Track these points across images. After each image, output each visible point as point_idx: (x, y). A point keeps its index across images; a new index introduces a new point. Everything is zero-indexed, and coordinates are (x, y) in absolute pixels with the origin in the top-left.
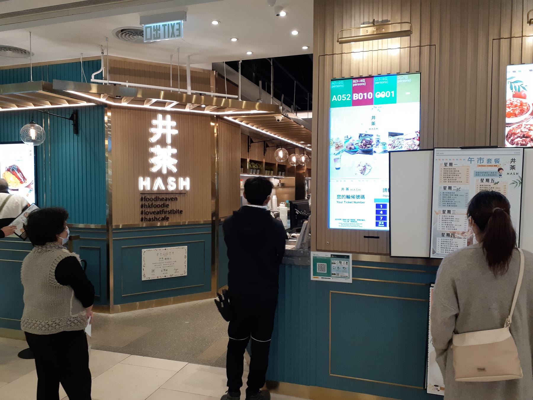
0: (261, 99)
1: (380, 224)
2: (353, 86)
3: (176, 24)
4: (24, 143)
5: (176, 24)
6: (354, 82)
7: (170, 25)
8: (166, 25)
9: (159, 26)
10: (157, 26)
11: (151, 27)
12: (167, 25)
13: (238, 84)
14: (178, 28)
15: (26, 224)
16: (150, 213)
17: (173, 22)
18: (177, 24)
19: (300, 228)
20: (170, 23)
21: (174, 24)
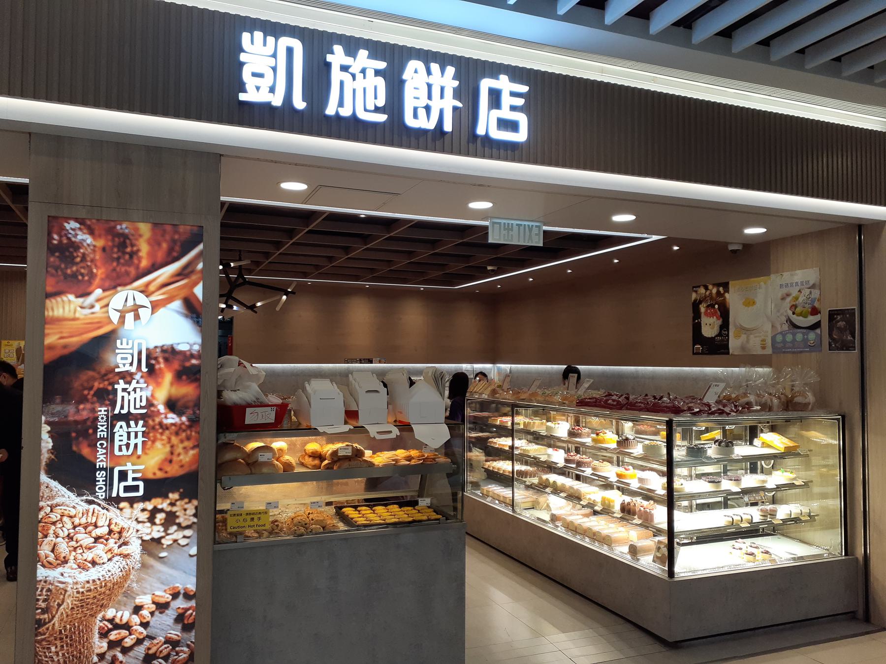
11: (500, 223)
12: (523, 225)
17: (531, 224)
18: (536, 226)
20: (527, 223)
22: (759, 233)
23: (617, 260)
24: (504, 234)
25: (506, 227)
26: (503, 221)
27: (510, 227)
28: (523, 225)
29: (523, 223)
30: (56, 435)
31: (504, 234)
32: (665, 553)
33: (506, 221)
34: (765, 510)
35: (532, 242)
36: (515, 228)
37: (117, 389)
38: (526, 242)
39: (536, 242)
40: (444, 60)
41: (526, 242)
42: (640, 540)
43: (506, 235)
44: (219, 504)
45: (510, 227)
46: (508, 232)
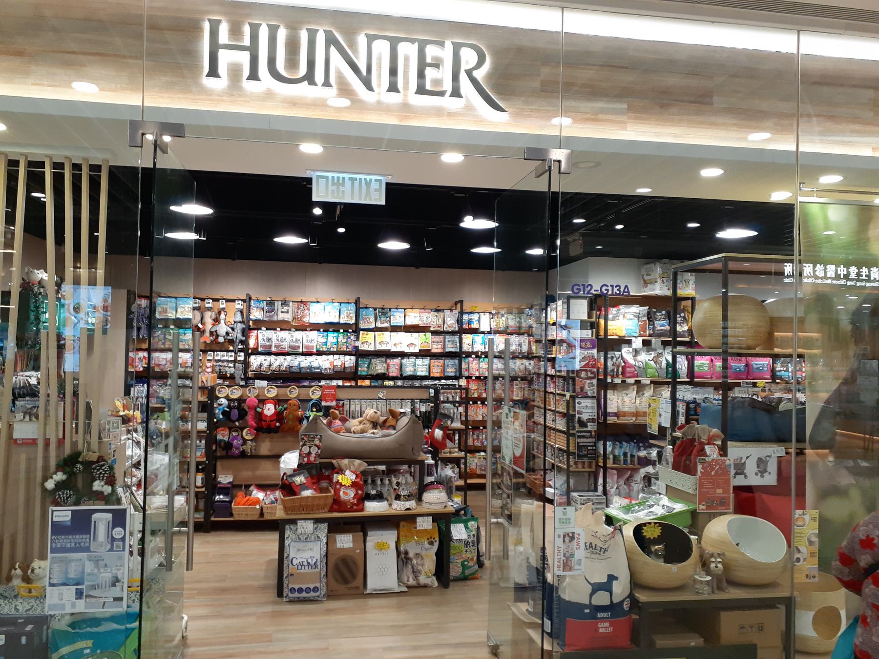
0: (859, 630)
1: (822, 278)
2: (711, 434)
3: (373, 180)
4: (778, 608)
5: (373, 180)
6: (181, 347)
7: (363, 180)
8: (356, 179)
9: (343, 178)
10: (338, 178)
11: (327, 178)
12: (358, 179)
13: (28, 235)
14: (306, 82)
15: (104, 502)
16: (802, 516)
17: (368, 177)
18: (376, 180)
19: (682, 468)
20: (363, 177)
21: (371, 180)
22: (826, 175)
23: (403, 238)
24: (333, 191)
25: (336, 182)
26: (330, 175)
27: (341, 182)
28: (358, 179)
29: (358, 176)
30: (778, 606)
31: (333, 191)
32: (362, 468)
33: (336, 175)
34: (519, 478)
35: (371, 200)
36: (348, 183)
37: (391, 189)
38: (363, 199)
39: (375, 200)
40: (143, 91)
41: (363, 199)
42: (37, 358)
43: (336, 191)
44: (371, 538)
45: (341, 182)
46: (338, 189)
